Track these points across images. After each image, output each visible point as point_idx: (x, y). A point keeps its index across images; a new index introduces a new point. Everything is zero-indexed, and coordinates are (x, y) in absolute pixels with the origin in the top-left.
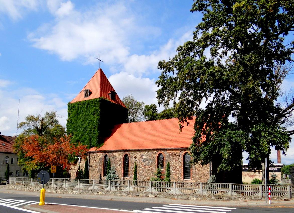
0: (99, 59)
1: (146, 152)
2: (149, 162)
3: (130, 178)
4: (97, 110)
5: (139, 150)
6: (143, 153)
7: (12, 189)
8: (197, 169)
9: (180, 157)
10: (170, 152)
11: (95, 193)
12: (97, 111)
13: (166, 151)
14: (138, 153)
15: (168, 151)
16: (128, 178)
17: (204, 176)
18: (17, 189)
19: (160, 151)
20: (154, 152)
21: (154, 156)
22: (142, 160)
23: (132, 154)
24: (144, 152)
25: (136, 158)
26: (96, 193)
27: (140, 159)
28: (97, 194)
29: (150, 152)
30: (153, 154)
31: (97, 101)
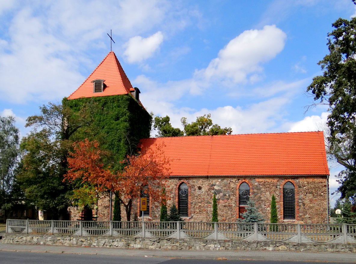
0: (111, 37)
1: (220, 180)
2: (225, 195)
3: (191, 218)
4: (123, 113)
5: (207, 177)
6: (214, 181)
7: (23, 242)
8: (306, 205)
9: (277, 188)
10: (261, 180)
11: (267, 248)
12: (124, 114)
13: (254, 179)
14: (204, 181)
15: (257, 180)
16: (188, 218)
17: (317, 214)
18: (42, 243)
19: (245, 179)
20: (234, 180)
21: (232, 185)
22: (213, 191)
23: (193, 182)
24: (215, 180)
25: (200, 188)
26: (271, 249)
27: (207, 190)
28: (274, 250)
29: (225, 181)
30: (231, 183)
31: (122, 99)
